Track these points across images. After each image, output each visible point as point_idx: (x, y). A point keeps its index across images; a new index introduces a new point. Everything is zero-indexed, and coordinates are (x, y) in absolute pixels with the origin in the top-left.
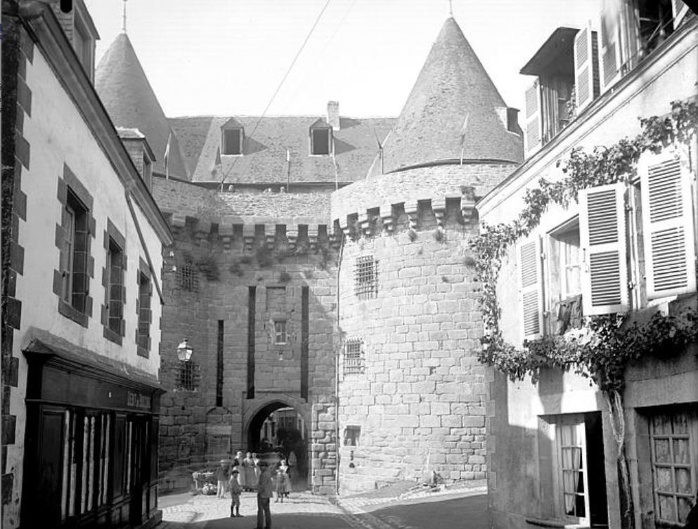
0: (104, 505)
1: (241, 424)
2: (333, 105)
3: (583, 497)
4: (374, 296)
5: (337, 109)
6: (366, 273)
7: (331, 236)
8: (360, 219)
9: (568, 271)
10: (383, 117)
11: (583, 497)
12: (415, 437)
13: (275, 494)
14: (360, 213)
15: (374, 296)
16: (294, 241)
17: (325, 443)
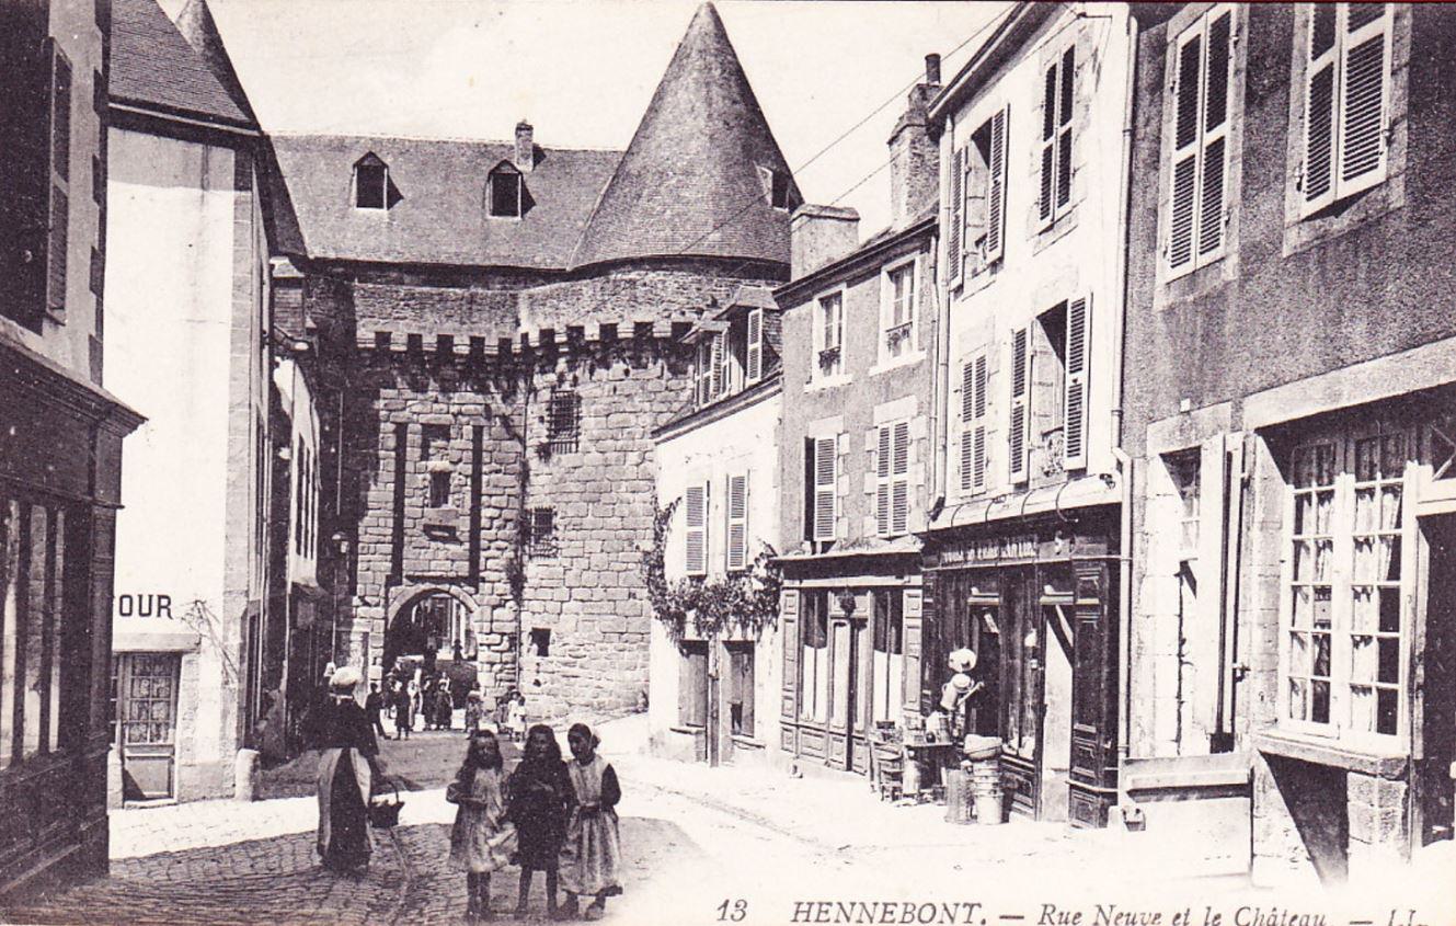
0: (55, 757)
1: (383, 622)
2: (524, 129)
3: (1395, 692)
4: (574, 449)
5: (531, 135)
6: (564, 415)
7: (515, 355)
8: (557, 339)
9: (529, 655)
10: (599, 149)
11: (1395, 692)
12: (621, 646)
13: (943, 769)
14: (557, 328)
15: (574, 449)
16: (462, 361)
17: (502, 652)
